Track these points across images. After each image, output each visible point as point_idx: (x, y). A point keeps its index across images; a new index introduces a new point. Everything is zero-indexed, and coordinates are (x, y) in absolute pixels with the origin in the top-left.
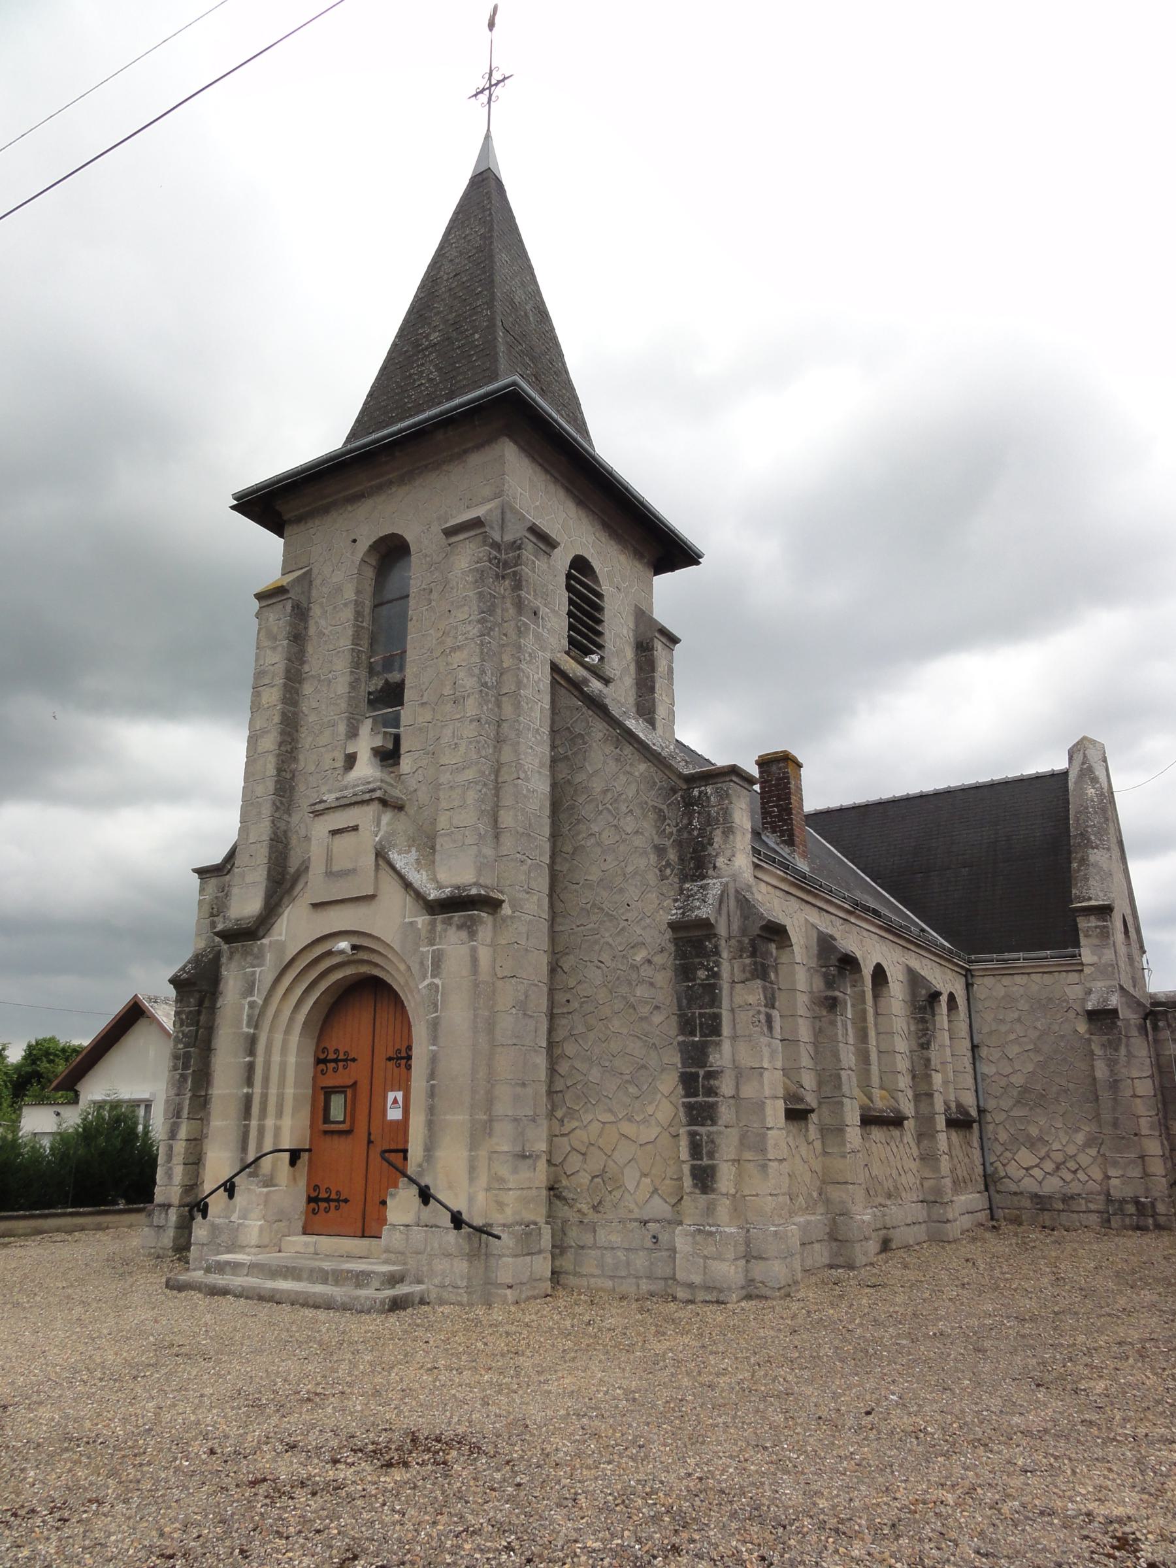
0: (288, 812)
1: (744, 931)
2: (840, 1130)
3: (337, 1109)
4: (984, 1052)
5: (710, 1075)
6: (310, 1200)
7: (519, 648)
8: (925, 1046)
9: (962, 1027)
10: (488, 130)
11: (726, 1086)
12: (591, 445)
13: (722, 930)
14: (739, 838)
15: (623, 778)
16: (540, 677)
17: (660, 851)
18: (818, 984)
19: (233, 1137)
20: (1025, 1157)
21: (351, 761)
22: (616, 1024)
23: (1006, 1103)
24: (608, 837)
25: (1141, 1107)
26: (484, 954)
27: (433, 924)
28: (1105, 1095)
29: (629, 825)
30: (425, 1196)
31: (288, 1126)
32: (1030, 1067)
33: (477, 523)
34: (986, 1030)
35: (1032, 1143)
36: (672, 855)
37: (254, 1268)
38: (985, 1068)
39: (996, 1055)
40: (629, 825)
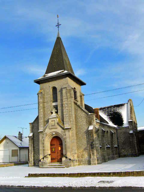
0: (45, 118)
1: (96, 130)
2: (105, 149)
3: (53, 150)
4: (119, 139)
5: (93, 144)
6: (51, 159)
7: (71, 101)
8: (112, 139)
9: (116, 136)
10: (58, 32)
11: (95, 145)
12: (74, 74)
13: (94, 130)
14: (65, 92)
15: (82, 114)
16: (73, 104)
17: (87, 122)
18: (102, 134)
19: (43, 153)
20: (123, 150)
21: (52, 113)
22: (83, 140)
23: (121, 144)
24: (81, 121)
25: (135, 144)
26: (70, 134)
27: (64, 131)
28: (131, 143)
29: (83, 119)
30: (66, 158)
31: (49, 152)
32: (123, 140)
33: (66, 88)
34: (119, 136)
35: (124, 149)
36: (88, 123)
37: (48, 166)
38: (119, 140)
39: (120, 139)
40: (83, 119)
